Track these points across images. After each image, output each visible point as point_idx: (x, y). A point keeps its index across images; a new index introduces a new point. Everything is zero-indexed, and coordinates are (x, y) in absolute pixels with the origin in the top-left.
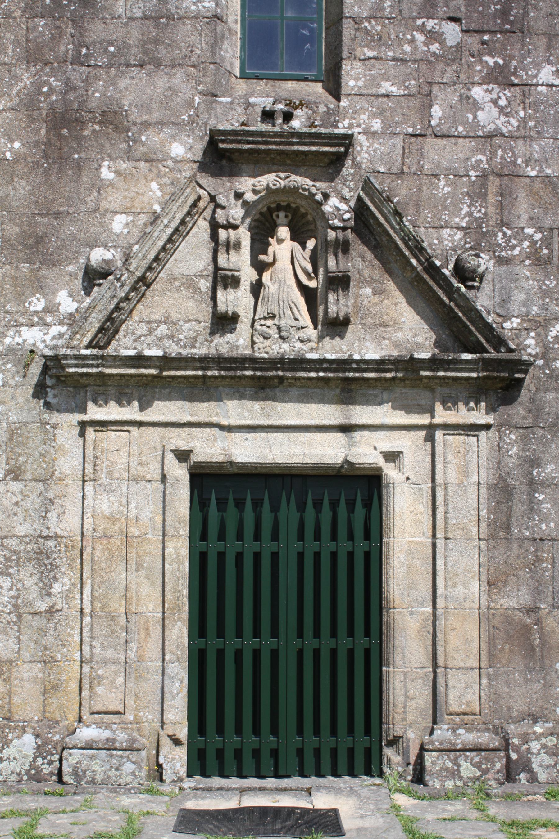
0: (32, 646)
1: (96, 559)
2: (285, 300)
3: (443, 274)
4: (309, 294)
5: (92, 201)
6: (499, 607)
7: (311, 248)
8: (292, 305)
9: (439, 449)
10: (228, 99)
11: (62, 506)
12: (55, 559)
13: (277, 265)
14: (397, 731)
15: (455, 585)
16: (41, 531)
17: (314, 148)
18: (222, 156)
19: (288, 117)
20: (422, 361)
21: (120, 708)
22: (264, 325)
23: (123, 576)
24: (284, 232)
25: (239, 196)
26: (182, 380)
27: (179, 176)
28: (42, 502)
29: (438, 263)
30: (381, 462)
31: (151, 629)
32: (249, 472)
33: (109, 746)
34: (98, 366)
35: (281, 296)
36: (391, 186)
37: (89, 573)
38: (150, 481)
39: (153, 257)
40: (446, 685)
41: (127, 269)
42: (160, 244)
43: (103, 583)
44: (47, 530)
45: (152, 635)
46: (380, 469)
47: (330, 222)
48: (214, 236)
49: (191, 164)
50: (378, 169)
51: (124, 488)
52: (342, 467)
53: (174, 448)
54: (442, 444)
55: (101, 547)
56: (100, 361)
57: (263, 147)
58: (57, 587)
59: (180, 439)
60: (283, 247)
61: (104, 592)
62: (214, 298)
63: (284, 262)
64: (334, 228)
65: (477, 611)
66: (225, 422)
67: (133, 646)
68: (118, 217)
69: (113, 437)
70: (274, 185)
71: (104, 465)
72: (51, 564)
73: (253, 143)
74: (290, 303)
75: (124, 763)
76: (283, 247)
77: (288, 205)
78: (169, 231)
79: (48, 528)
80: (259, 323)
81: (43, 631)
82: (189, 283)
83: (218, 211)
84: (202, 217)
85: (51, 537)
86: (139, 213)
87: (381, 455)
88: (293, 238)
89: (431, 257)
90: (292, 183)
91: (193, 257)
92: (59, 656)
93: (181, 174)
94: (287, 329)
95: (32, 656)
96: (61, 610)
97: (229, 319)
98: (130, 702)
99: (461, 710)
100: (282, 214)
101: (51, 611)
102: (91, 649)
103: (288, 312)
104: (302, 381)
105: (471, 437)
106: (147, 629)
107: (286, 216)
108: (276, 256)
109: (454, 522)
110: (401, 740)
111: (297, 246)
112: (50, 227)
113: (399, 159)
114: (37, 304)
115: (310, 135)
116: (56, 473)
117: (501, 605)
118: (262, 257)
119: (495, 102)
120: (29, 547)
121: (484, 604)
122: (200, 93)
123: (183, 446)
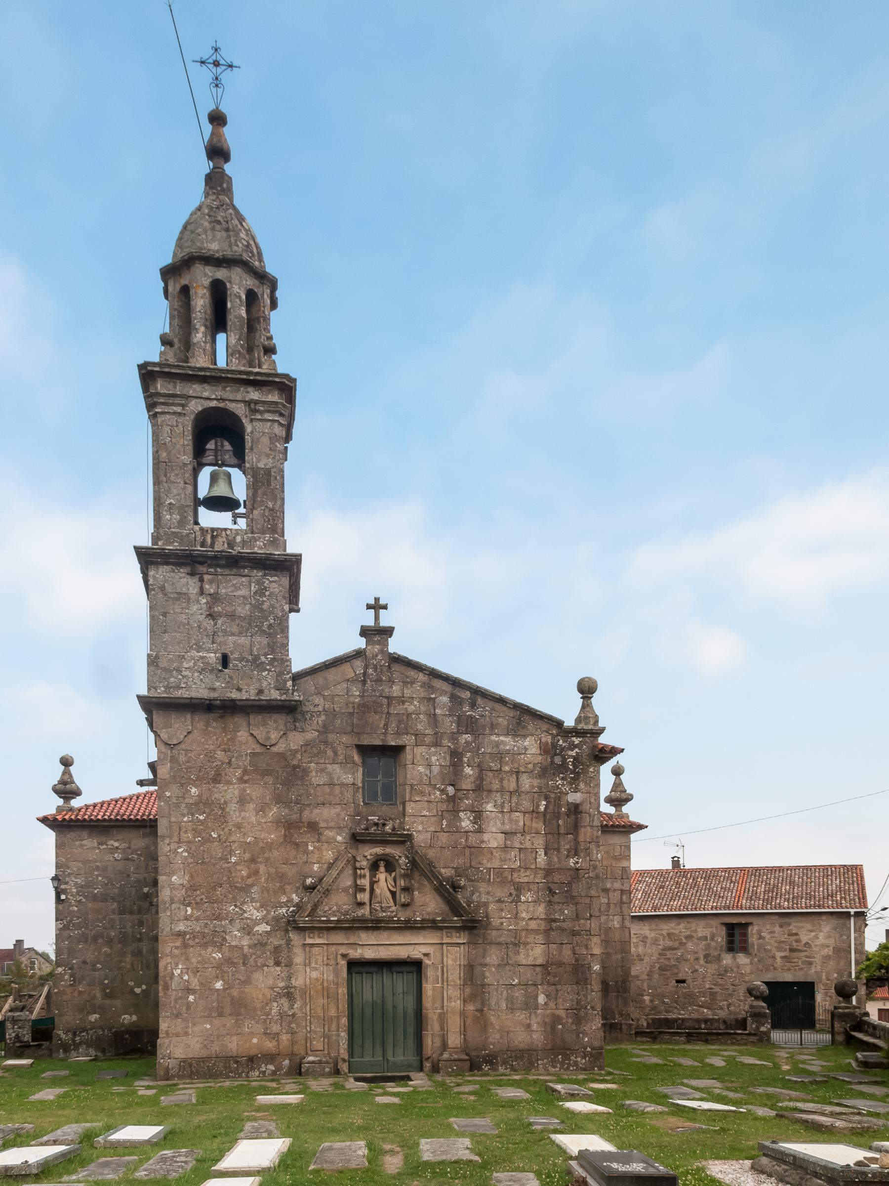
4: (393, 894)
9: (445, 952)
18: (357, 839)
19: (384, 825)
24: (382, 869)
25: (366, 857)
30: (422, 957)
33: (320, 1062)
58: (296, 1006)
59: (343, 950)
60: (382, 876)
62: (356, 897)
63: (382, 883)
69: (316, 950)
76: (382, 876)
81: (290, 1023)
82: (345, 890)
88: (387, 871)
101: (293, 1015)
114: (284, 899)
119: (469, 819)
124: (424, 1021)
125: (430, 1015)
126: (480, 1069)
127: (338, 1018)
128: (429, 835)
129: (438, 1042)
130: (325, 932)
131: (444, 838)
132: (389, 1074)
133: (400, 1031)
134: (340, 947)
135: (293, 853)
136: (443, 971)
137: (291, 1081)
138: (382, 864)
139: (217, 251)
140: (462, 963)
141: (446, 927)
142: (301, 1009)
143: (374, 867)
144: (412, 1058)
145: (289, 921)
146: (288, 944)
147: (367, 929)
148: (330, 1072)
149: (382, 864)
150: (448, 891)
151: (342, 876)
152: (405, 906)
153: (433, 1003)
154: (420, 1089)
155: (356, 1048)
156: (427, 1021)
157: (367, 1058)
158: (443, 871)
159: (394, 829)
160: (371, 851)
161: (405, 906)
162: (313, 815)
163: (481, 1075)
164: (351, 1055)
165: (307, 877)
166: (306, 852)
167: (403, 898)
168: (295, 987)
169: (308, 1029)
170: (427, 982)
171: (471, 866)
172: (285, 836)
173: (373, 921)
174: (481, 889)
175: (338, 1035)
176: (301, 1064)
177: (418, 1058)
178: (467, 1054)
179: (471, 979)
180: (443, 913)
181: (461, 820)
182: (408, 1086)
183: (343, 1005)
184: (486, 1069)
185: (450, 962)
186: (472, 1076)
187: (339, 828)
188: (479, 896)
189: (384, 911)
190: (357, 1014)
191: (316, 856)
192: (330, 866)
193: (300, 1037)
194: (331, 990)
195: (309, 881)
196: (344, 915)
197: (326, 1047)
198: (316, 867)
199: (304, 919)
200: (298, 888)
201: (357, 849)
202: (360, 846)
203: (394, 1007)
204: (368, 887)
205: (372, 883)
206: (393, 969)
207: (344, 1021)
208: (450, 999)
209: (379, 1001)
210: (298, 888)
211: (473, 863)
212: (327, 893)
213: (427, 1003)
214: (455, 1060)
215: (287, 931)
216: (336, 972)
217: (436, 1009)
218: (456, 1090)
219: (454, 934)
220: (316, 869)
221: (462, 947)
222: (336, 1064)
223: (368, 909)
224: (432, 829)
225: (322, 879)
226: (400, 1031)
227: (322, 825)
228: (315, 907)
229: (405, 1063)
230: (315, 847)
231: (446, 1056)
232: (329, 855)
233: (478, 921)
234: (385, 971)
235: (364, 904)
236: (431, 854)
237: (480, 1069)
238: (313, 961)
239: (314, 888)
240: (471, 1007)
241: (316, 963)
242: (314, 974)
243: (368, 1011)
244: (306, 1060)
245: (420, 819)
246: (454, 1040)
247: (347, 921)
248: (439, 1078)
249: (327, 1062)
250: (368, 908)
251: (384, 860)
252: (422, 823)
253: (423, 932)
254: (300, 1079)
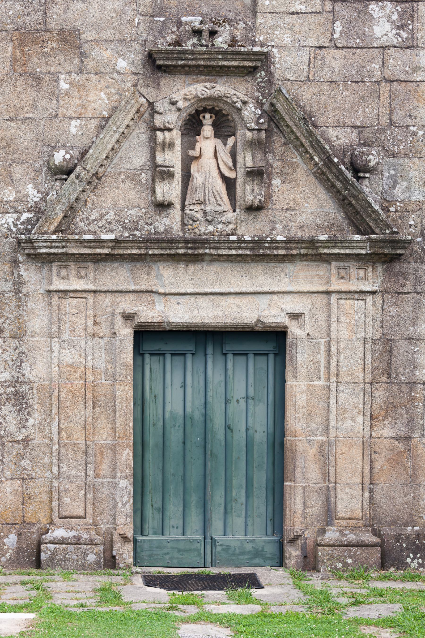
0: (13, 467)
1: (62, 399)
2: (210, 189)
3: (340, 169)
4: (230, 184)
6: (380, 436)
7: (232, 144)
8: (216, 194)
9: (334, 311)
10: (162, 19)
11: (34, 358)
12: (29, 399)
13: (203, 159)
14: (296, 532)
15: (344, 419)
16: (18, 378)
17: (235, 63)
18: (158, 65)
19: (213, 33)
21: (82, 514)
22: (193, 210)
23: (83, 413)
24: (208, 130)
25: (173, 103)
26: (128, 257)
27: (123, 86)
28: (18, 355)
30: (287, 321)
31: (105, 453)
32: (181, 329)
33: (77, 541)
34: (63, 247)
37: (57, 410)
38: (102, 337)
40: (336, 497)
43: (67, 418)
44: (22, 377)
45: (106, 458)
46: (286, 327)
47: (248, 125)
48: (153, 140)
49: (133, 76)
50: (288, 77)
51: (83, 343)
52: (256, 325)
53: (121, 312)
54: (336, 308)
55: (65, 390)
57: (192, 63)
58: (31, 421)
59: (127, 304)
60: (207, 143)
61: (69, 425)
63: (208, 160)
64: (251, 130)
65: (362, 439)
66: (162, 291)
67: (91, 466)
68: (73, 122)
69: (71, 303)
70: (203, 95)
71: (67, 325)
72: (26, 403)
73: (186, 59)
74: (214, 191)
75: (88, 554)
76: (207, 143)
78: (117, 135)
79: (23, 375)
80: (189, 208)
81: (21, 456)
82: (132, 177)
83: (156, 116)
85: (26, 382)
86: (91, 119)
87: (287, 316)
88: (216, 135)
89: (330, 155)
90: (217, 92)
92: (34, 474)
93: (124, 85)
94: (212, 214)
95: (13, 474)
96: (34, 439)
98: (90, 509)
99: (348, 516)
101: (26, 441)
102: (59, 468)
103: (212, 199)
104: (225, 257)
105: (360, 301)
106: (102, 452)
107: (211, 117)
108: (202, 151)
109: (345, 369)
110: (300, 538)
111: (218, 142)
112: (18, 130)
113: (306, 69)
116: (28, 332)
117: (381, 435)
118: (191, 153)
120: (8, 391)
121: (367, 434)
122: (140, 14)
123: (129, 310)
124: (288, 453)
125: (301, 447)
126: (401, 565)
127: (114, 448)
128: (304, 54)
129: (316, 508)
131: (336, 61)
132: (215, 571)
133: (239, 480)
134: (120, 298)
135: (29, 95)
136: (329, 352)
137: (17, 578)
138: (208, 120)
139: (299, 271)
140: (369, 335)
141: (338, 257)
142: (41, 428)
143: (192, 126)
144: (262, 538)
145: (19, 242)
146: (17, 291)
147: (175, 259)
148: (97, 563)
149: (208, 120)
150: (344, 177)
151: (126, 144)
152: (253, 209)
153: (308, 421)
154: (275, 610)
155: (149, 513)
156: (294, 460)
157: (172, 535)
158: (332, 133)
159: (233, 42)
161: (253, 209)
162: (70, 15)
163: (404, 579)
164: (140, 527)
165: (54, 148)
166: (55, 95)
167: (249, 193)
168: (29, 383)
169: (55, 470)
170: (295, 375)
171: (391, 123)
172: (15, 60)
173: (187, 241)
174: (413, 174)
175: (114, 486)
176: (39, 543)
177: (275, 538)
178: (376, 533)
179: (388, 371)
180: (330, 227)
181: (372, 21)
182: (249, 600)
183: (126, 422)
184: (414, 565)
185: (344, 333)
186: (386, 578)
187: (122, 41)
188: (408, 188)
190: (152, 440)
191: (75, 102)
192: (104, 122)
193: (38, 488)
194: (101, 390)
195: (59, 157)
197: (90, 509)
198: (74, 127)
199: (47, 239)
200: (38, 171)
201: (157, 86)
202: (164, 81)
203: (228, 428)
204: (178, 171)
205: (188, 162)
206: (227, 348)
207: (127, 455)
208: (342, 412)
209: (198, 415)
210: (38, 171)
213: (296, 420)
214: (350, 545)
215: (15, 263)
216: (112, 352)
217: (314, 433)
218: (353, 613)
219: (353, 271)
220: (73, 130)
221: (370, 298)
222: (109, 545)
223: (178, 218)
224: (312, 41)
225: (86, 152)
226: (239, 480)
227: (88, 35)
229: (249, 547)
230: (72, 85)
231: (331, 535)
232: (100, 101)
233: (405, 244)
234: (210, 350)
235: (170, 205)
236: (308, 96)
237: (401, 565)
238: (66, 327)
239: (69, 173)
240: (385, 431)
241: (72, 332)
242: (69, 356)
243: (175, 437)
244: (48, 537)
245: (288, 19)
246: (350, 502)
247: (135, 241)
248: (316, 582)
249: (92, 543)
250: (176, 213)
251: (212, 111)
252: (292, 29)
253: (289, 267)
254: (36, 576)
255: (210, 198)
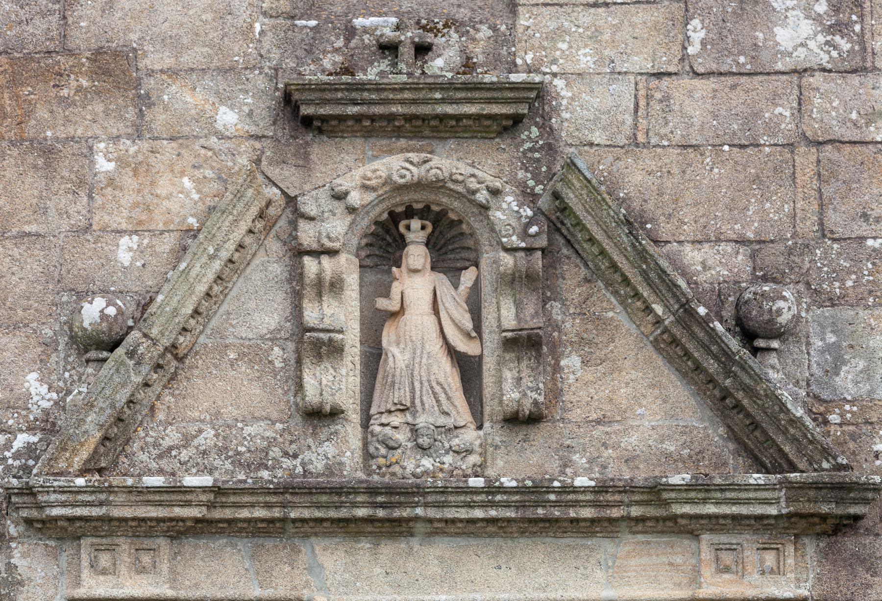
2: (424, 379)
3: (713, 329)
4: (468, 369)
5: (79, 213)
7: (470, 284)
8: (438, 389)
13: (407, 316)
17: (472, 109)
18: (305, 116)
19: (422, 50)
20: (674, 488)
24: (417, 254)
25: (339, 197)
27: (230, 164)
29: (702, 311)
34: (101, 504)
35: (416, 373)
36: (615, 168)
39: (189, 311)
41: (145, 335)
42: (202, 288)
47: (504, 240)
48: (296, 276)
49: (252, 142)
50: (589, 138)
56: (103, 497)
60: (417, 284)
62: (300, 386)
63: (418, 320)
74: (434, 384)
76: (417, 284)
77: (427, 208)
80: (378, 422)
82: (254, 354)
83: (302, 224)
84: (273, 232)
86: (162, 233)
90: (434, 171)
91: (258, 310)
93: (233, 161)
97: (325, 416)
100: (416, 224)
103: (429, 401)
108: (406, 299)
111: (442, 281)
113: (629, 120)
115: (467, 87)
118: (382, 303)
122: (265, 14)
130: (124, 545)
131: (694, 104)
135: (30, 187)
138: (416, 232)
139: (628, 556)
141: (715, 523)
143: (383, 245)
147: (348, 528)
149: (416, 232)
150: (722, 348)
151: (239, 286)
152: (521, 421)
158: (692, 256)
160: (363, 173)
161: (521, 421)
165: (83, 296)
166: (85, 184)
167: (511, 384)
171: (823, 232)
173: (373, 491)
187: (227, 71)
189: (423, 450)
191: (128, 199)
195: (93, 312)
196: (248, 467)
198: (125, 250)
199: (68, 487)
200: (49, 345)
201: (304, 163)
202: (321, 150)
204: (352, 339)
205: (375, 323)
210: (49, 345)
211: (833, 218)
212: (174, 360)
219: (751, 555)
220: (124, 257)
224: (641, 62)
227: (155, 59)
228: (118, 433)
230: (122, 162)
232: (181, 194)
235: (335, 414)
236: (636, 178)
250: (351, 432)
251: (425, 213)
252: (595, 36)
253: (605, 547)
255: (424, 398)
